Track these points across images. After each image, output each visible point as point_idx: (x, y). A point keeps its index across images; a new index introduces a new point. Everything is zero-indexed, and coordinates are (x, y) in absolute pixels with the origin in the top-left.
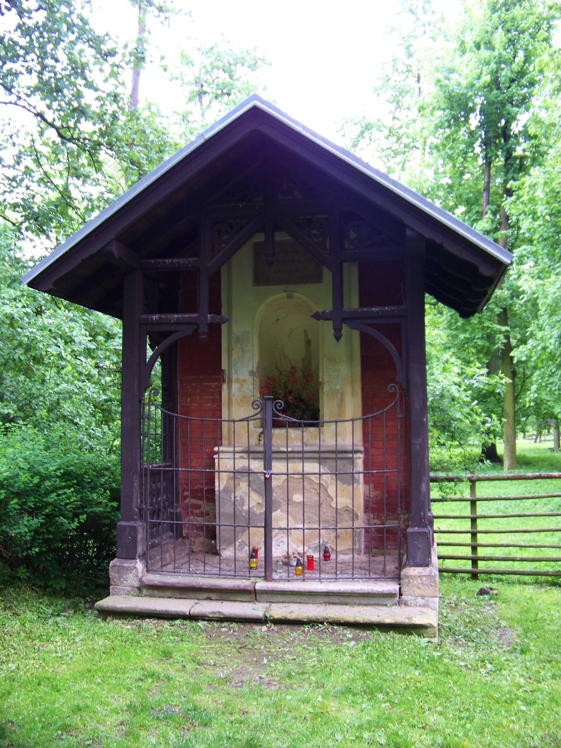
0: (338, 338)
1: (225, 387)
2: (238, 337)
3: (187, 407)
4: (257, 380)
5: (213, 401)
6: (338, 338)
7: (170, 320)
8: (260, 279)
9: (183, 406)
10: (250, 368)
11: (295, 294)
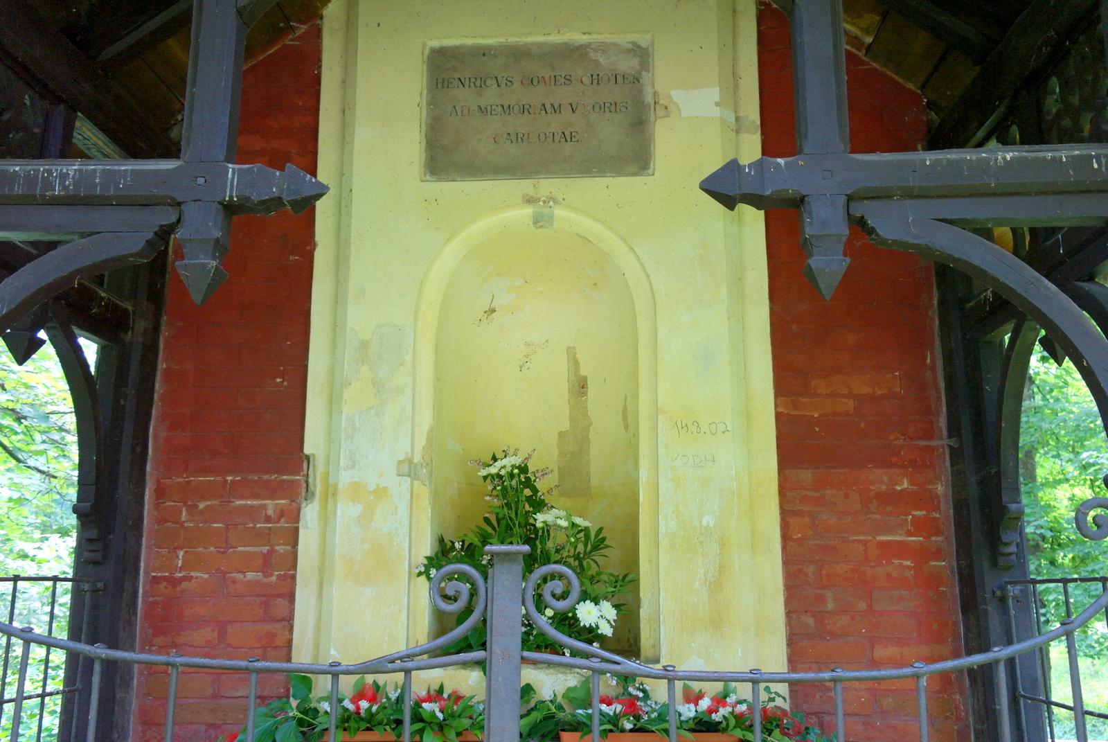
0: (477, 526)
1: (310, 513)
2: (364, 345)
3: (173, 582)
4: (424, 493)
5: (267, 563)
6: (477, 526)
7: (48, 184)
8: (444, 157)
9: (156, 580)
10: (403, 448)
11: (559, 212)
